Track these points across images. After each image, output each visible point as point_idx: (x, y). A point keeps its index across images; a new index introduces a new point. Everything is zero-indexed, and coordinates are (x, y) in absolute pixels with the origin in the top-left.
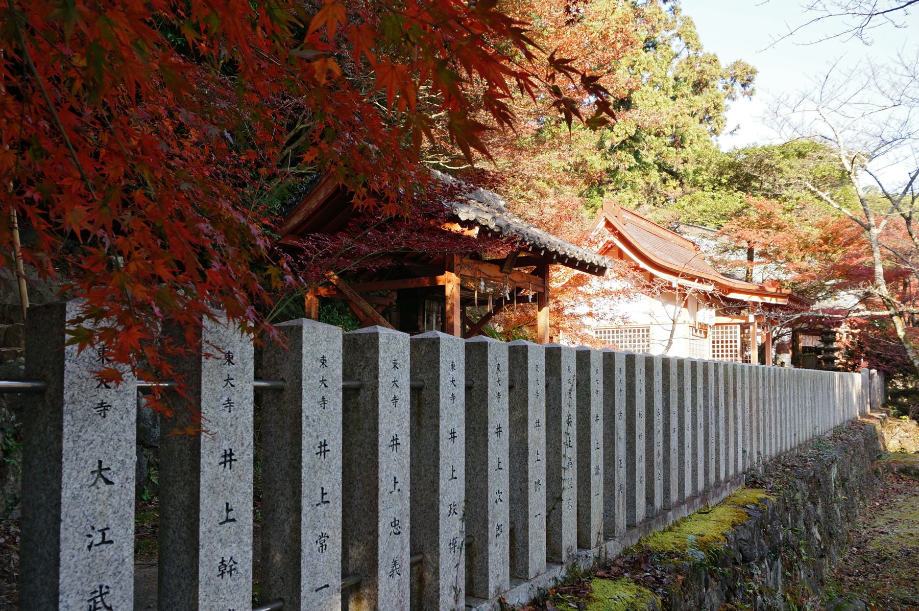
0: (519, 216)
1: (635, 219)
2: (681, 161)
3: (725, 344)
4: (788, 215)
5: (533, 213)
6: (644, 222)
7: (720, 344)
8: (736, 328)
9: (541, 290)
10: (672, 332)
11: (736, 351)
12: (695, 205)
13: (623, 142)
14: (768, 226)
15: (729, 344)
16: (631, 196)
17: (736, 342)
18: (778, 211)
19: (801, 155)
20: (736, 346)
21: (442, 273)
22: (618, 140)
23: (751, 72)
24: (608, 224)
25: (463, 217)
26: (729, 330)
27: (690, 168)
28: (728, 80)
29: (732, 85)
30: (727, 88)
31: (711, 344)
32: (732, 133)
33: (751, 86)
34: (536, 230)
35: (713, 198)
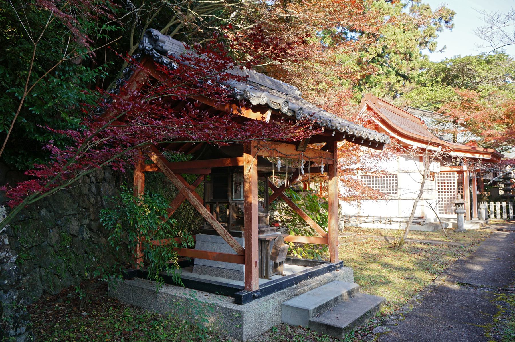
0: (312, 103)
1: (385, 105)
2: (411, 69)
3: (449, 184)
4: (482, 100)
5: (321, 100)
6: (391, 106)
7: (443, 185)
8: (454, 174)
9: (330, 163)
10: (423, 184)
11: (454, 189)
12: (421, 95)
13: (374, 58)
14: (469, 108)
15: (446, 185)
16: (379, 91)
17: (454, 183)
18: (476, 98)
19: (488, 62)
20: (454, 186)
21: (241, 155)
22: (371, 57)
23: (452, 14)
24: (369, 108)
25: (254, 102)
26: (449, 175)
27: (415, 73)
28: (437, 19)
29: (440, 22)
30: (436, 24)
31: (437, 185)
32: (441, 51)
33: (452, 22)
34: (325, 113)
35: (432, 90)
